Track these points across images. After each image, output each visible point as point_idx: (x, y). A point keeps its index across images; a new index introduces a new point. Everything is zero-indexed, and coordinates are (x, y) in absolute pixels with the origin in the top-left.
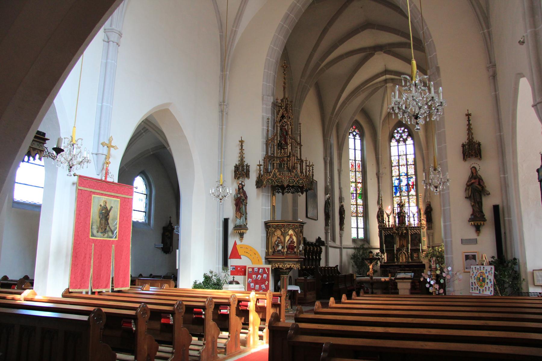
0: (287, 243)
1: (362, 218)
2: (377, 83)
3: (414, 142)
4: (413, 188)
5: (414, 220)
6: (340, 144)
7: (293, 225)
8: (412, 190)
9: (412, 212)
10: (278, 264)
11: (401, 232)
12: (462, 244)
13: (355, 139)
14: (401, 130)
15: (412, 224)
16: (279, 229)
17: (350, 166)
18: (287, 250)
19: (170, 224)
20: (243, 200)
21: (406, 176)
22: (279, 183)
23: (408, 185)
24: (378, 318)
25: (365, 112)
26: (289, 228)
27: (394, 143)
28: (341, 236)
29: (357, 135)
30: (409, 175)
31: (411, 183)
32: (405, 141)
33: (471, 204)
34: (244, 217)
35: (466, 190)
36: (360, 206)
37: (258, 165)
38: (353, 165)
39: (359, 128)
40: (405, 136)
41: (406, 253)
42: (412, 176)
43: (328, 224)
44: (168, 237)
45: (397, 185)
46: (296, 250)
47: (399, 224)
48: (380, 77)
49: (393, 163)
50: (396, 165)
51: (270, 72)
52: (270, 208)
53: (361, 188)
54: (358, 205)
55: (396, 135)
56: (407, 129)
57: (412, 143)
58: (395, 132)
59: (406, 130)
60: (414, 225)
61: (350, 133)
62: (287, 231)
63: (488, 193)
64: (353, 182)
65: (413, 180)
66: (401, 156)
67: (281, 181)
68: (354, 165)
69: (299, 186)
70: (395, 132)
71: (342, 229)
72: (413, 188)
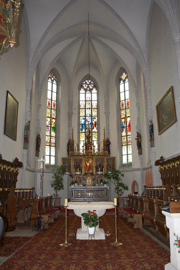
13: (52, 83)
14: (88, 81)
21: (90, 117)
27: (82, 91)
29: (54, 81)
30: (93, 116)
32: (91, 90)
36: (53, 138)
38: (50, 103)
42: (95, 117)
45: (83, 123)
49: (81, 106)
50: (83, 108)
58: (84, 83)
59: (92, 82)
68: (51, 103)
70: (84, 83)
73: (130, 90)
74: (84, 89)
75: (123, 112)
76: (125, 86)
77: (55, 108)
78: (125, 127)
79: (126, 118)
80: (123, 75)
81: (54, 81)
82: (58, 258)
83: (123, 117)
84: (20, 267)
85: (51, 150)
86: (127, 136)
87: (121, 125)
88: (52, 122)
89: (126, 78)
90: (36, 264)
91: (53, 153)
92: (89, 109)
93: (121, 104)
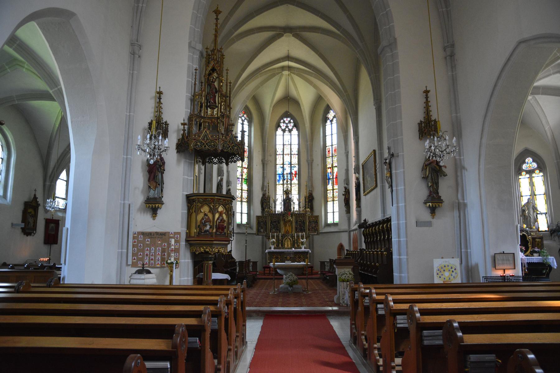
0: (216, 221)
2: (274, 69)
4: (296, 177)
7: (224, 200)
8: (295, 178)
10: (203, 248)
12: (417, 226)
14: (287, 120)
16: (208, 205)
18: (217, 231)
19: (35, 198)
20: (160, 166)
22: (211, 147)
24: (155, 290)
25: (256, 100)
26: (220, 204)
27: (279, 132)
29: (245, 120)
31: (293, 172)
32: (290, 131)
33: (428, 184)
34: (160, 187)
35: (422, 170)
37: (182, 124)
39: (248, 113)
40: (291, 126)
41: (291, 239)
42: (295, 165)
44: (31, 214)
45: (280, 173)
46: (225, 230)
48: (280, 62)
49: (277, 151)
51: (199, 15)
52: (193, 178)
55: (282, 125)
56: (293, 121)
57: (297, 134)
58: (281, 121)
59: (292, 121)
62: (217, 207)
63: (446, 174)
64: (240, 167)
65: (296, 169)
66: (286, 145)
67: (214, 145)
69: (234, 153)
70: (281, 121)
72: (296, 177)
74: (282, 130)
75: (329, 161)
79: (332, 167)
81: (245, 120)
86: (333, 190)
87: (327, 176)
89: (334, 117)
91: (245, 210)
93: (327, 151)
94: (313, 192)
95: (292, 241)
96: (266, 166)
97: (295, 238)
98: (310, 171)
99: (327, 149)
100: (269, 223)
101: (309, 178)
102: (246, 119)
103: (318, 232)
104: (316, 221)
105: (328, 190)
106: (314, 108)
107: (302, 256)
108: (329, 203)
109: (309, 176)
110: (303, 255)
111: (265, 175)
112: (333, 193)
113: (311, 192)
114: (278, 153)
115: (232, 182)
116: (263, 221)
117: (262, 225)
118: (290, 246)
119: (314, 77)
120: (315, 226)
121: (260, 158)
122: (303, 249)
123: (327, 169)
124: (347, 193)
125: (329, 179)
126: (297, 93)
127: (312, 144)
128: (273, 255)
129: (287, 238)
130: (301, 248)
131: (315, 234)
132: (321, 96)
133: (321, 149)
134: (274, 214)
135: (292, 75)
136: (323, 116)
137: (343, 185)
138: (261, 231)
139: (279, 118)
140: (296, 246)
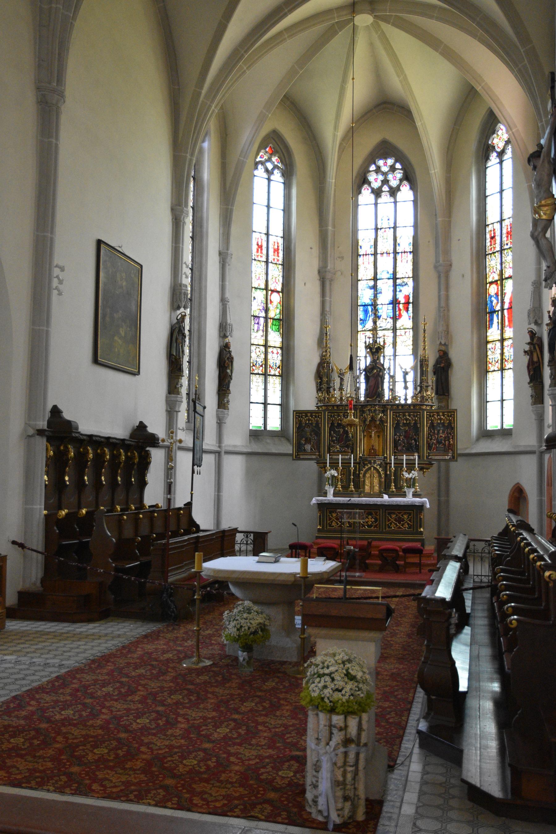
1: (278, 381)
3: (415, 196)
4: (407, 310)
5: (406, 388)
6: (228, 185)
8: (404, 313)
9: (402, 368)
11: (372, 417)
14: (385, 164)
15: (400, 397)
17: (255, 247)
23: (395, 302)
28: (220, 423)
29: (276, 171)
31: (401, 297)
32: (393, 192)
36: (275, 350)
40: (394, 180)
42: (405, 280)
43: (176, 387)
45: (368, 302)
47: (366, 396)
49: (361, 247)
53: (279, 306)
54: (270, 347)
55: (372, 177)
56: (401, 164)
57: (412, 199)
59: (398, 166)
60: (406, 399)
61: (256, 164)
64: (260, 289)
65: (407, 290)
66: (383, 230)
68: (264, 245)
70: (371, 169)
71: (224, 404)
72: (407, 310)
73: (516, 188)
74: (373, 191)
75: (493, 263)
76: (504, 171)
77: (278, 260)
78: (498, 311)
80: (500, 133)
81: (276, 171)
82: (285, 712)
83: (493, 278)
84: (153, 756)
85: (269, 387)
86: (502, 340)
87: (487, 304)
88: (271, 302)
89: (508, 142)
90: (227, 721)
91: (275, 396)
92: (388, 253)
93: (488, 236)
94: (450, 350)
95: (383, 476)
96: (330, 284)
97: (390, 467)
98: (443, 293)
99: (487, 231)
100: (325, 427)
101: (439, 311)
102: (278, 168)
103: (453, 453)
104: (450, 423)
105: (488, 342)
106: (455, 124)
107: (405, 517)
108: (490, 376)
109: (439, 307)
110: (410, 514)
111: (327, 309)
112: (502, 348)
113: (443, 348)
114: (361, 252)
115: (234, 327)
116: (312, 424)
117: (308, 434)
118: (377, 488)
119: (439, 19)
120: (445, 438)
121: (315, 264)
122: (409, 499)
123: (488, 285)
124: (535, 348)
125: (493, 312)
126: (401, 81)
127: (449, 223)
128: (330, 512)
129: (370, 468)
130: (404, 495)
131: (447, 457)
132: (473, 87)
133: (472, 231)
134: (338, 406)
135: (383, 25)
136: (480, 142)
137: (526, 326)
138: (305, 450)
139: (364, 162)
140: (393, 488)
